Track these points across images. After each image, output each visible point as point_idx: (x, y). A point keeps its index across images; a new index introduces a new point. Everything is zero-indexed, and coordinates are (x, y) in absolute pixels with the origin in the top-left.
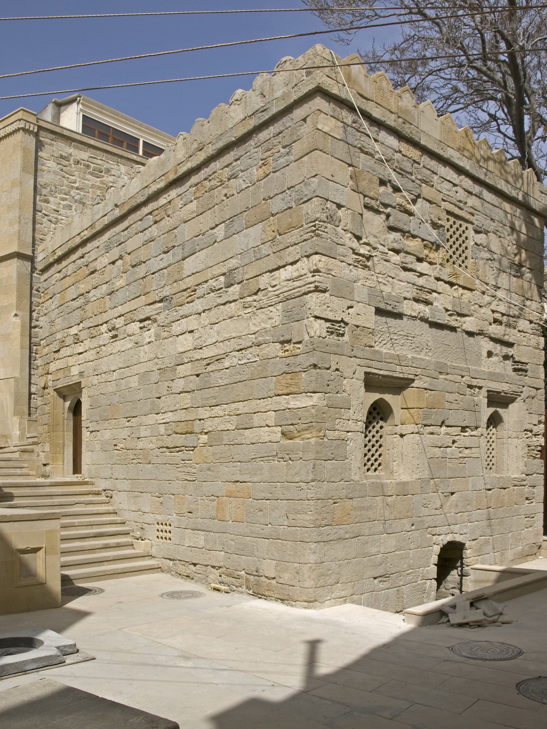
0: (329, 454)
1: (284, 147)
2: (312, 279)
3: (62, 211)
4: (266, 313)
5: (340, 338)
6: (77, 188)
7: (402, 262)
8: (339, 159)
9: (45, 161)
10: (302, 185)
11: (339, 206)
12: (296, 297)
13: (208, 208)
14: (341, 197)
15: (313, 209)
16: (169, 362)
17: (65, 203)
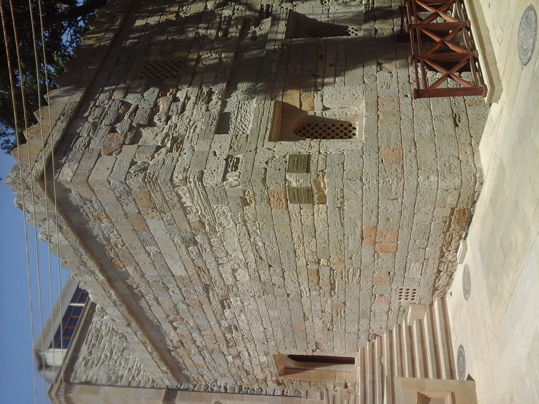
0: (338, 167)
2: (192, 184)
3: (130, 365)
5: (241, 160)
7: (177, 114)
8: (95, 164)
9: (89, 377)
10: (115, 191)
11: (133, 163)
12: (207, 194)
15: (135, 183)
16: (257, 287)
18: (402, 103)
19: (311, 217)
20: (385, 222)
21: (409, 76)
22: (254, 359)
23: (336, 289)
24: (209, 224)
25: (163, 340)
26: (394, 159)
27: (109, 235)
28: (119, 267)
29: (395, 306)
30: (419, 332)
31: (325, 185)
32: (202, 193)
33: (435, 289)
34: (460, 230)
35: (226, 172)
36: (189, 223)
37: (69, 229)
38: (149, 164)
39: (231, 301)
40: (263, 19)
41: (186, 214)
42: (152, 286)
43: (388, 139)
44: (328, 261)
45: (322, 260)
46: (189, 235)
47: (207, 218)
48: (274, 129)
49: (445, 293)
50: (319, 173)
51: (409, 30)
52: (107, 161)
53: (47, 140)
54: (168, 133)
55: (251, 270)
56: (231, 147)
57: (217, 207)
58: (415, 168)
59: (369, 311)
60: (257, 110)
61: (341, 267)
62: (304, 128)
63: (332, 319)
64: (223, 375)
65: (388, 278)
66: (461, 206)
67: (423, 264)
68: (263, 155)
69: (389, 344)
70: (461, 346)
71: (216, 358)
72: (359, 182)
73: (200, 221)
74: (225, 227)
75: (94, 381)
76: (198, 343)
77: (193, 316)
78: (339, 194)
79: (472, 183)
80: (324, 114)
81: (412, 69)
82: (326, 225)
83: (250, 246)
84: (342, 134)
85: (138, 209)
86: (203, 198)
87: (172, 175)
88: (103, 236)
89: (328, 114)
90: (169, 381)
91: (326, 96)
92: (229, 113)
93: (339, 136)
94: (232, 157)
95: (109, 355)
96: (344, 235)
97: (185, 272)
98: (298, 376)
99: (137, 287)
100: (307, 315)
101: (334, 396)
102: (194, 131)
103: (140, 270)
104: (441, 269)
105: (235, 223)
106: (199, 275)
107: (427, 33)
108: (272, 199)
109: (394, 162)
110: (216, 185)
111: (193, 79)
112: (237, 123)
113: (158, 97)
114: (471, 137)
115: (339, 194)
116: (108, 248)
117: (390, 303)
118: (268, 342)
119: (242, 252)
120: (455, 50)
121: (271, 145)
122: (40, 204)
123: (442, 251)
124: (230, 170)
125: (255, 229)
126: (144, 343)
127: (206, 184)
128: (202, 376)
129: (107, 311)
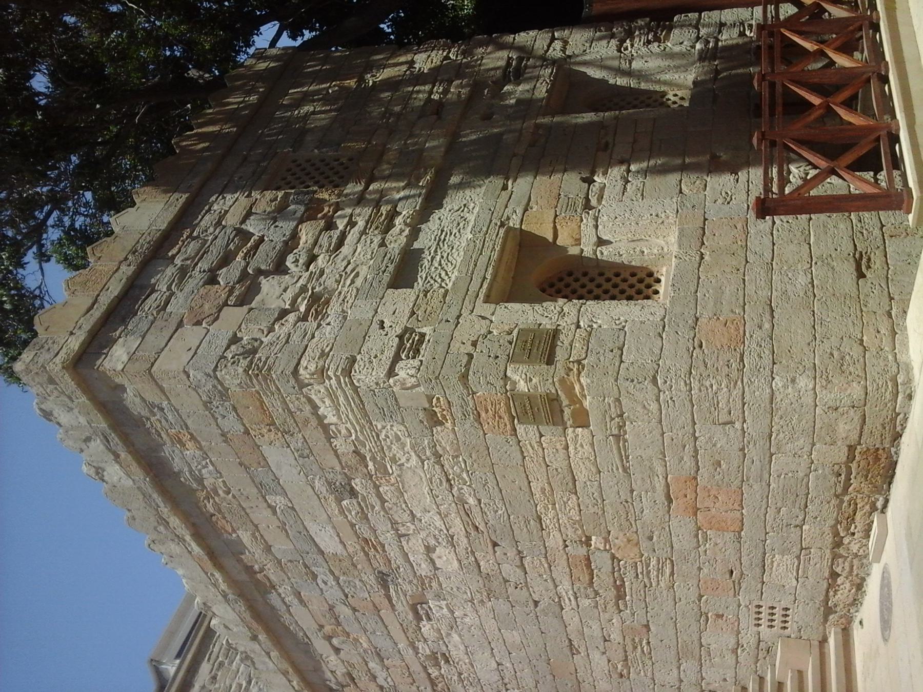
0: (611, 355)
4: (389, 443)
5: (427, 338)
7: (327, 252)
8: (169, 341)
11: (235, 340)
12: (362, 401)
13: (245, 516)
14: (221, 337)
15: (232, 376)
16: (475, 584)
18: (752, 231)
19: (562, 452)
20: (711, 469)
24: (373, 459)
25: (318, 669)
26: (725, 341)
27: (200, 471)
28: (226, 531)
29: (748, 638)
31: (583, 390)
32: (353, 399)
33: (828, 611)
34: (872, 492)
35: (397, 358)
36: (337, 456)
37: (130, 458)
38: (262, 342)
39: (429, 607)
41: (329, 438)
43: (718, 302)
44: (606, 540)
45: (593, 538)
46: (339, 477)
47: (368, 447)
48: (499, 279)
49: (850, 621)
50: (571, 366)
52: (191, 335)
53: (98, 295)
54: (306, 286)
55: (461, 550)
56: (413, 313)
57: (384, 428)
58: (767, 361)
59: (697, 645)
60: (472, 244)
61: (632, 555)
62: (561, 280)
63: (626, 657)
65: (730, 582)
66: (868, 441)
67: (798, 557)
68: (470, 327)
72: (650, 387)
73: (356, 452)
76: (380, 681)
77: (365, 631)
78: (613, 409)
79: (888, 396)
80: (598, 253)
82: (594, 470)
83: (453, 505)
84: (632, 292)
85: (244, 425)
86: (355, 409)
87: (298, 364)
89: (605, 253)
91: (603, 219)
92: (421, 251)
93: (556, 287)
95: (244, 685)
96: (632, 491)
97: (340, 547)
99: (262, 570)
100: (575, 643)
102: (353, 282)
103: (262, 539)
105: (420, 457)
106: (367, 555)
107: (792, 87)
108: (483, 414)
109: (726, 347)
110: (377, 384)
112: (433, 269)
113: (301, 221)
114: (891, 299)
115: (613, 409)
116: (202, 495)
117: (739, 633)
119: (440, 515)
120: (852, 120)
121: (485, 309)
122: (76, 411)
123: (836, 534)
124: (403, 357)
125: (458, 471)
126: (285, 673)
127: (358, 381)
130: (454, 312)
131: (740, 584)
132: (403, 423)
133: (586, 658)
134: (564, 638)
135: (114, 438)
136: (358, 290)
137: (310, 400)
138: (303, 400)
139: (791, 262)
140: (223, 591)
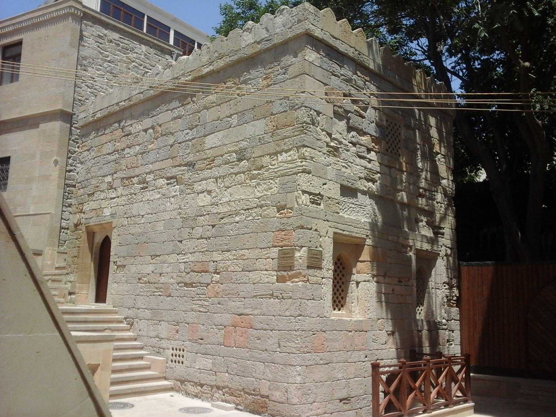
1: (282, 68)
2: (300, 164)
5: (318, 207)
6: (109, 62)
11: (318, 113)
15: (302, 115)
16: (191, 212)
17: (99, 73)
19: (264, 268)
21: (382, 360)
22: (107, 203)
23: (186, 288)
24: (259, 174)
25: (132, 117)
27: (250, 84)
29: (164, 343)
30: (139, 367)
33: (182, 382)
34: (246, 404)
35: (310, 194)
36: (260, 156)
38: (317, 127)
39: (174, 186)
40: (433, 229)
41: (270, 155)
42: (194, 115)
43: (332, 340)
45: (218, 276)
51: (425, 360)
53: (339, 40)
56: (329, 198)
58: (308, 363)
59: (160, 319)
61: (210, 293)
62: (341, 264)
63: (151, 283)
64: (88, 171)
66: (271, 404)
67: (211, 370)
68: (323, 227)
69: (125, 337)
70: (133, 406)
71: (109, 165)
72: (297, 313)
73: (263, 167)
74: (256, 188)
75: (83, 43)
76: (127, 150)
78: (286, 295)
81: (395, 362)
82: (255, 281)
86: (285, 171)
87: (308, 147)
88: (249, 79)
89: (353, 286)
90: (83, 116)
91: (368, 284)
92: (357, 197)
94: (321, 199)
95: (108, 59)
96: (244, 298)
97: (209, 147)
98: (85, 245)
99: (194, 102)
101: (61, 281)
102: (343, 166)
103: (212, 104)
104: (205, 387)
106: (205, 159)
108: (283, 233)
110: (299, 185)
111: (385, 166)
113: (371, 136)
114: (331, 414)
115: (286, 295)
116: (237, 80)
117: (168, 340)
118: (127, 218)
121: (331, 234)
122: (283, 28)
123: (224, 388)
124: (311, 197)
126: (129, 99)
128: (88, 150)
129: (168, 70)
130: (330, 219)
131: (196, 342)
132: (278, 193)
133: (149, 262)
134: (160, 253)
135: (268, 45)
136: (340, 170)
137: (290, 150)
138: (290, 147)
139: (348, 370)
140: (180, 78)
